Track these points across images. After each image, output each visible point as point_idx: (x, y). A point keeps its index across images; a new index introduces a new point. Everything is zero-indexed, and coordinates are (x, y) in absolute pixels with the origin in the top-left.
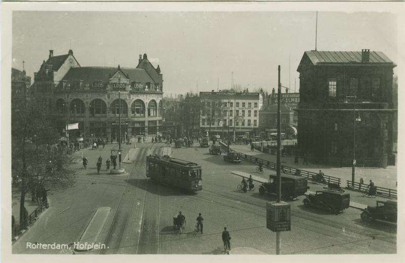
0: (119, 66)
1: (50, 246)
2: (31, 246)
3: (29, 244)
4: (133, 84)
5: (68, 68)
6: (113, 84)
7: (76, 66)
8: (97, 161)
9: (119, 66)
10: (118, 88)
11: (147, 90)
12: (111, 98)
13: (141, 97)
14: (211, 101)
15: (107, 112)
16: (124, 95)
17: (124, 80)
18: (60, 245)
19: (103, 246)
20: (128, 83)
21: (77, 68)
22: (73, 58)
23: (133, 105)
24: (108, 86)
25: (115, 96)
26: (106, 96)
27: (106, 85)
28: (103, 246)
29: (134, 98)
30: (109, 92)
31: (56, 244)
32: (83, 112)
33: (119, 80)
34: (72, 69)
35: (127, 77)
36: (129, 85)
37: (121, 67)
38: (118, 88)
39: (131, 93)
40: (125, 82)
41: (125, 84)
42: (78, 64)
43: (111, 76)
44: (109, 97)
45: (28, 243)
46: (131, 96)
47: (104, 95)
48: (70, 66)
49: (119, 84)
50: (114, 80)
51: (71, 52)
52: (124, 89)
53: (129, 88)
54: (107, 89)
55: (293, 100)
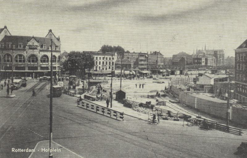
0: (159, 52)
1: (25, 151)
2: (15, 150)
3: (13, 149)
4: (42, 46)
5: (4, 36)
6: (29, 46)
7: (9, 35)
8: (144, 87)
9: (159, 52)
10: (32, 48)
11: (50, 49)
12: (28, 54)
13: (10, 52)
14: (102, 57)
15: (26, 62)
16: (36, 52)
17: (36, 44)
18: (30, 150)
19: (60, 150)
20: (38, 45)
21: (10, 36)
22: (7, 30)
23: (42, 58)
24: (27, 47)
25: (31, 52)
26: (25, 52)
27: (24, 47)
28: (60, 150)
29: (43, 53)
30: (27, 50)
31: (29, 149)
32: (24, 61)
33: (33, 43)
34: (6, 36)
35: (38, 42)
36: (39, 46)
37: (34, 36)
38: (32, 48)
39: (41, 51)
40: (37, 45)
41: (37, 46)
42: (10, 34)
43: (28, 41)
44: (27, 53)
45: (12, 148)
46: (41, 53)
47: (24, 52)
48: (5, 34)
49: (33, 45)
50: (30, 43)
51: (6, 27)
52: (36, 49)
53: (39, 48)
54: (26, 48)
55: (134, 56)
